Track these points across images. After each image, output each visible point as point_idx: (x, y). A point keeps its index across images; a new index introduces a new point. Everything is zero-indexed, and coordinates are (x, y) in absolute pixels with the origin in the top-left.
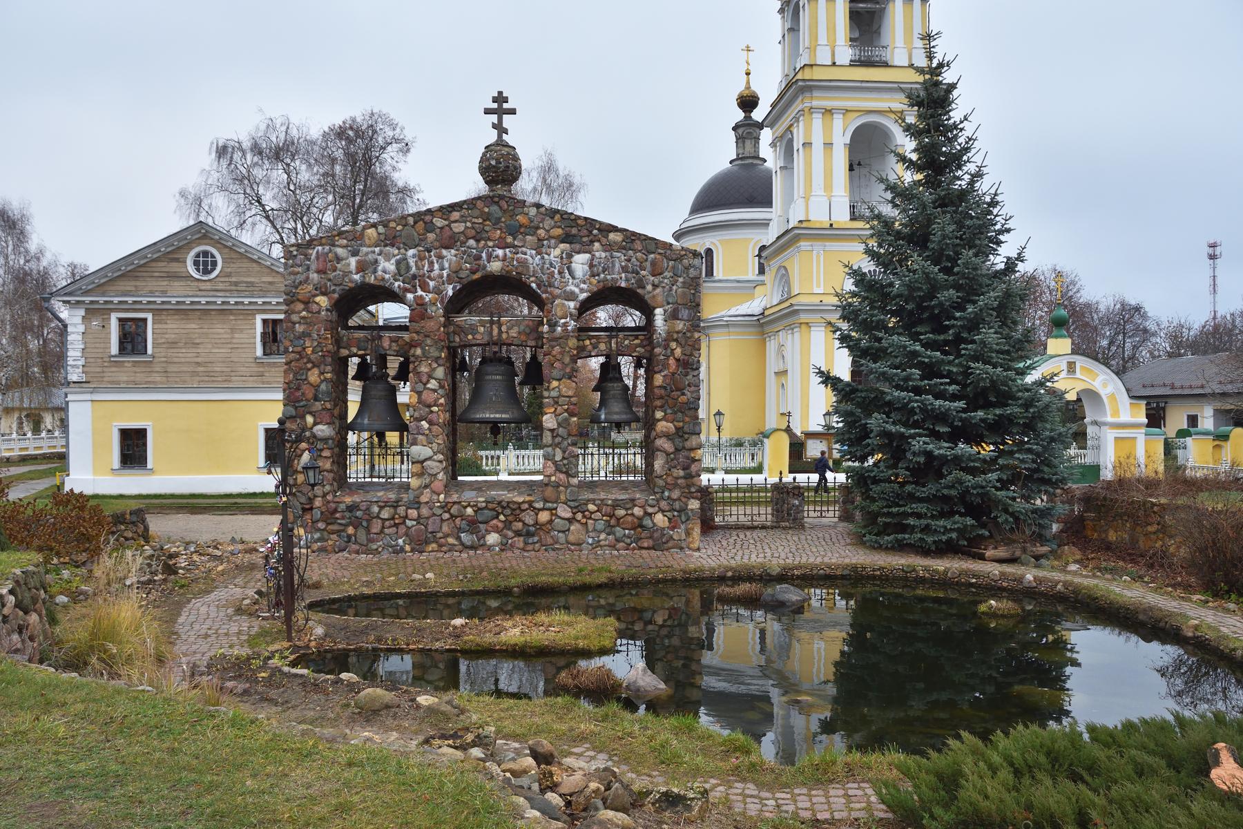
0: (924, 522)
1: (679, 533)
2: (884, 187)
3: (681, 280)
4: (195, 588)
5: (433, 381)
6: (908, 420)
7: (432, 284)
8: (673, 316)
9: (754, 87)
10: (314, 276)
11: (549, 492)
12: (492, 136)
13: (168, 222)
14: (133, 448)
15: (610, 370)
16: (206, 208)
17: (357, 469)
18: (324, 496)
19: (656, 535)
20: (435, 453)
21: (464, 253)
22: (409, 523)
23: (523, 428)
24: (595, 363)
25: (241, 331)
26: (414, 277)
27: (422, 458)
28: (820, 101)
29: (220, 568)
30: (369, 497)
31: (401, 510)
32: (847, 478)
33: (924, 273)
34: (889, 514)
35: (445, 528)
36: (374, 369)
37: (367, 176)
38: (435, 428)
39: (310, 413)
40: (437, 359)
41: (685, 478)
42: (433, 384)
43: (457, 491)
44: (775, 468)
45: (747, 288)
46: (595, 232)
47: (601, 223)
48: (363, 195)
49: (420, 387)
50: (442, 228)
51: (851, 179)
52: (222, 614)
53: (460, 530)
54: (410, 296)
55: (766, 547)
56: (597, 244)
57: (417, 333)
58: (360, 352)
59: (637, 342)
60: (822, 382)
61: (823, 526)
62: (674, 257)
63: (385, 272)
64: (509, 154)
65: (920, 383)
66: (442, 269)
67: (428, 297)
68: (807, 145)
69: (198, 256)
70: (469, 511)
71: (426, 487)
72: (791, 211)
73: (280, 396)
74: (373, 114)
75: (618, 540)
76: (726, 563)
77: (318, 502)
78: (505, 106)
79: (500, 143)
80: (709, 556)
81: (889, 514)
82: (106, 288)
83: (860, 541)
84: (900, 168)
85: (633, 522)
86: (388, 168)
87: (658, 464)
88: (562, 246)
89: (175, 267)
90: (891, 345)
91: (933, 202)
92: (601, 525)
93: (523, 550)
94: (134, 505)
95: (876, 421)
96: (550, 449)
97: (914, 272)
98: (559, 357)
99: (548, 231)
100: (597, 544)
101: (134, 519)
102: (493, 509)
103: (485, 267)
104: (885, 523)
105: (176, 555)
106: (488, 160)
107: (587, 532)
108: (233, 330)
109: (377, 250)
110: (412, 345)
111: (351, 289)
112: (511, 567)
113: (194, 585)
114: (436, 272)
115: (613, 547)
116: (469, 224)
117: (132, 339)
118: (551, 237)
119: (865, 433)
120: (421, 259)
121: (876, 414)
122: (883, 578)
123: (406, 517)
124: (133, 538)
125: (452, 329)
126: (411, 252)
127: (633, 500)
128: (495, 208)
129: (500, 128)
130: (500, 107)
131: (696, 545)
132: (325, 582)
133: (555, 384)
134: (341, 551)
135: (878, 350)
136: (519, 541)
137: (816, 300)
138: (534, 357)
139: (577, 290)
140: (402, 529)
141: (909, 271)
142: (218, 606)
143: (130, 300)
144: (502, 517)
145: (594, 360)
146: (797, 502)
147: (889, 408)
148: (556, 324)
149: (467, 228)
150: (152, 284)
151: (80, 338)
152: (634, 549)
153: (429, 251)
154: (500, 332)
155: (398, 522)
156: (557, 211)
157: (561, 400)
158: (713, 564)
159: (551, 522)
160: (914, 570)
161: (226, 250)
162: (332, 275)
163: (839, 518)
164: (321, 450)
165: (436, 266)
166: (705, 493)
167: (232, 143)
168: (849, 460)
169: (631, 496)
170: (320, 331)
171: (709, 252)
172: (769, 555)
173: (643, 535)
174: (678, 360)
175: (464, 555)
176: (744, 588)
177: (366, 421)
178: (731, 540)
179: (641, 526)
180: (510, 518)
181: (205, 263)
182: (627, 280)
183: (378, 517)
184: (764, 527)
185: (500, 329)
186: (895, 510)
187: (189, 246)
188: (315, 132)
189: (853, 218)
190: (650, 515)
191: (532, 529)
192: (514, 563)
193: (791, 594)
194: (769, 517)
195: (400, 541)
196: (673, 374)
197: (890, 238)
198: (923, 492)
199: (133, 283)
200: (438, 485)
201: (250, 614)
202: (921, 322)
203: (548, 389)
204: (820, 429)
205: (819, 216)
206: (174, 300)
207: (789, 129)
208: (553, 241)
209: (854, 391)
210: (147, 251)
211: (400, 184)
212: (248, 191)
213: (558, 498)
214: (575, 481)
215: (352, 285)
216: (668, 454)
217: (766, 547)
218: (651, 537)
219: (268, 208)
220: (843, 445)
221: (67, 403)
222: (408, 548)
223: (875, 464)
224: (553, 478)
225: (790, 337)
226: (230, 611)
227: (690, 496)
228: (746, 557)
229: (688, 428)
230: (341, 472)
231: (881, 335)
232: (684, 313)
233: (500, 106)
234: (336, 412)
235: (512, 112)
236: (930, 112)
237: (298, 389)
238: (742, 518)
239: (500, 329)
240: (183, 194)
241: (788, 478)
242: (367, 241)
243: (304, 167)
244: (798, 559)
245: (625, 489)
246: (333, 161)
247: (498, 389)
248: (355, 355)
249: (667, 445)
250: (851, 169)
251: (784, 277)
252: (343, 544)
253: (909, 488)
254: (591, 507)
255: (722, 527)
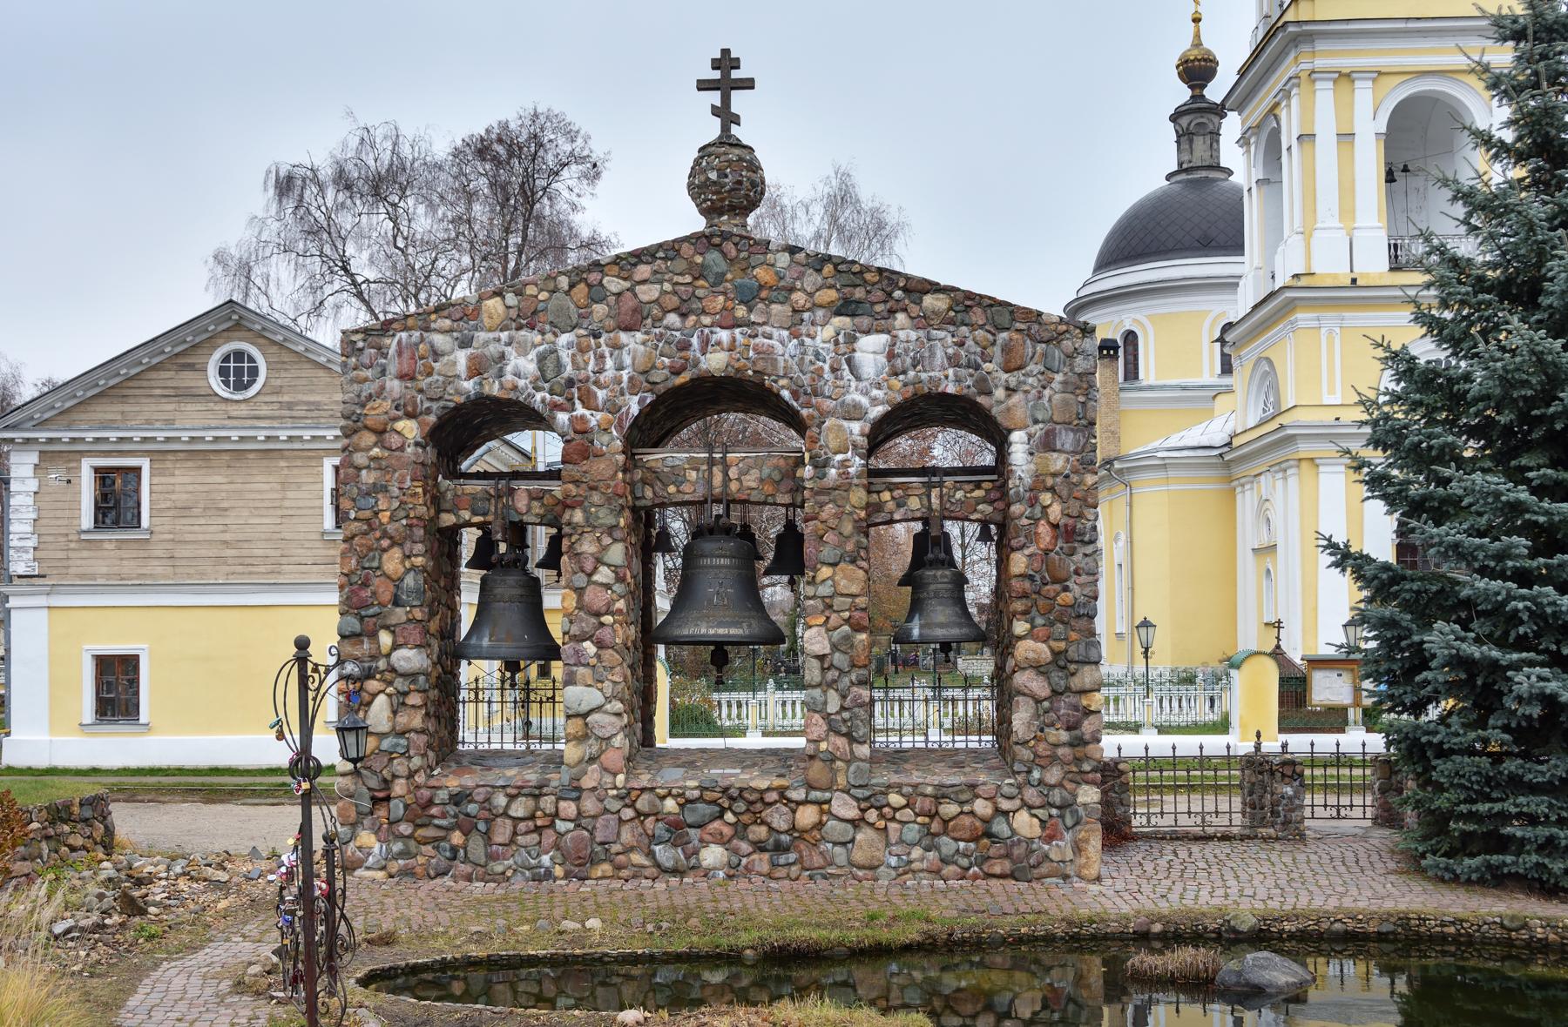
0: (1543, 832)
1: (1060, 849)
2: (1449, 194)
3: (1059, 377)
4: (173, 940)
5: (603, 569)
6: (1506, 633)
7: (601, 394)
8: (1047, 444)
9: (1208, 43)
10: (394, 386)
11: (817, 770)
12: (711, 129)
13: (196, 298)
14: (116, 689)
15: (931, 548)
16: (258, 281)
17: (484, 725)
18: (411, 775)
19: (1016, 852)
20: (608, 700)
21: (660, 337)
22: (561, 826)
23: (772, 653)
24: (903, 533)
25: (299, 485)
26: (570, 383)
27: (584, 708)
28: (1328, 58)
29: (222, 905)
30: (493, 777)
31: (547, 803)
32: (1388, 745)
33: (1533, 352)
34: (1471, 816)
35: (627, 836)
36: (503, 548)
37: (527, 220)
38: (608, 654)
39: (387, 628)
40: (611, 530)
41: (1071, 745)
42: (604, 574)
43: (648, 768)
44: (1253, 723)
45: (1201, 399)
46: (898, 294)
47: (908, 278)
48: (520, 253)
49: (580, 580)
50: (619, 295)
51: (1390, 197)
52: (209, 991)
53: (653, 838)
54: (562, 417)
55: (1229, 875)
56: (901, 317)
57: (576, 482)
58: (477, 519)
59: (978, 493)
60: (1336, 565)
61: (1342, 836)
62: (1046, 336)
63: (518, 375)
64: (741, 159)
65: (1528, 563)
66: (620, 368)
67: (595, 419)
68: (1306, 138)
69: (226, 359)
70: (670, 805)
71: (592, 760)
72: (1278, 259)
73: (334, 598)
74: (536, 115)
75: (945, 861)
76: (1149, 906)
77: (399, 787)
78: (735, 74)
79: (726, 140)
80: (1116, 892)
81: (1471, 816)
82: (75, 416)
83: (1413, 865)
84: (1480, 158)
85: (973, 828)
86: (562, 206)
87: (1021, 719)
88: (838, 321)
89: (188, 379)
90: (1469, 491)
91: (1550, 219)
92: (912, 832)
93: (769, 876)
94: (89, 788)
95: (1440, 637)
96: (817, 693)
97: (1513, 351)
98: (832, 523)
99: (811, 295)
100: (906, 868)
101: (88, 813)
102: (714, 802)
103: (696, 363)
104: (1464, 833)
105: (149, 880)
106: (704, 171)
107: (888, 844)
108: (284, 485)
109: (504, 336)
110: (567, 504)
111: (458, 408)
112: (744, 909)
113: (171, 935)
114: (610, 373)
115: (936, 873)
116: (667, 287)
117: (115, 502)
118: (816, 306)
119: (1421, 660)
120: (583, 350)
121: (1439, 624)
122: (1464, 940)
123: (556, 815)
124: (84, 848)
125: (638, 474)
126: (564, 339)
127: (973, 786)
128: (713, 256)
129: (726, 115)
130: (726, 77)
131: (1092, 872)
132: (403, 932)
133: (825, 572)
134: (438, 875)
135: (1445, 501)
136: (762, 862)
137: (1327, 417)
138: (790, 526)
139: (865, 401)
140: (549, 837)
141: (1503, 349)
142: (204, 977)
143: (113, 435)
144: (729, 817)
145: (900, 528)
146: (1289, 791)
147: (1463, 610)
148: (826, 464)
149: (664, 293)
150: (149, 409)
151: (30, 501)
152: (975, 877)
153: (597, 336)
154: (727, 479)
155: (541, 824)
156: (828, 259)
157: (838, 601)
158: (1126, 909)
159: (819, 825)
160: (1525, 926)
161: (275, 349)
162: (424, 383)
163: (1375, 819)
164: (405, 694)
165: (609, 363)
166: (1111, 774)
167: (302, 171)
168: (1390, 710)
169: (970, 779)
170: (404, 481)
171: (1130, 337)
172: (1234, 891)
173: (992, 852)
174: (1055, 526)
175: (660, 886)
176: (1183, 958)
177: (486, 642)
178: (1163, 862)
179: (988, 834)
180: (746, 818)
181: (239, 372)
182: (958, 380)
183: (505, 814)
184: (1225, 838)
185: (726, 474)
186: (1483, 807)
187: (212, 342)
188: (441, 149)
189: (1396, 266)
190: (1006, 813)
191: (785, 838)
192: (750, 901)
193: (1277, 971)
194: (1237, 819)
195: (546, 859)
196: (1047, 552)
197: (1463, 289)
198: (1540, 773)
199: (120, 407)
200: (614, 758)
201: (258, 993)
202: (1527, 446)
203: (812, 582)
204: (1331, 652)
205: (1330, 265)
206: (185, 436)
207: (1272, 112)
208: (820, 313)
209: (1397, 579)
210: (141, 353)
211: (585, 233)
212: (327, 249)
213: (833, 781)
214: (863, 751)
215: (462, 399)
216: (1038, 701)
217: (1229, 875)
218: (1008, 856)
219: (360, 279)
220: (1378, 681)
221: (9, 611)
222: (558, 871)
223: (1443, 720)
224: (823, 746)
225: (1279, 484)
226: (225, 986)
227: (1081, 778)
228: (1190, 895)
229: (1074, 655)
230: (444, 733)
231: (1447, 472)
232: (1066, 439)
233: (726, 75)
234: (434, 626)
235: (748, 84)
236: (1540, 48)
237: (365, 584)
238: (1184, 820)
239: (726, 474)
240: (220, 258)
241: (1272, 745)
242: (487, 321)
243: (421, 209)
244: (1291, 900)
245: (959, 765)
246: (470, 197)
247: (721, 585)
248: (469, 524)
249: (1039, 686)
250: (1390, 178)
251: (1268, 377)
252: (444, 863)
253: (1511, 766)
254: (895, 799)
255: (1147, 837)
